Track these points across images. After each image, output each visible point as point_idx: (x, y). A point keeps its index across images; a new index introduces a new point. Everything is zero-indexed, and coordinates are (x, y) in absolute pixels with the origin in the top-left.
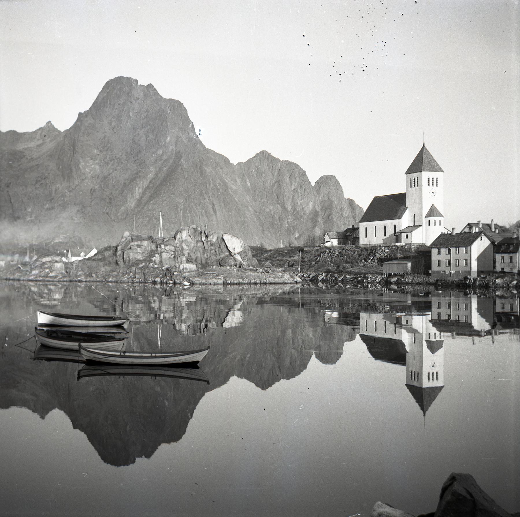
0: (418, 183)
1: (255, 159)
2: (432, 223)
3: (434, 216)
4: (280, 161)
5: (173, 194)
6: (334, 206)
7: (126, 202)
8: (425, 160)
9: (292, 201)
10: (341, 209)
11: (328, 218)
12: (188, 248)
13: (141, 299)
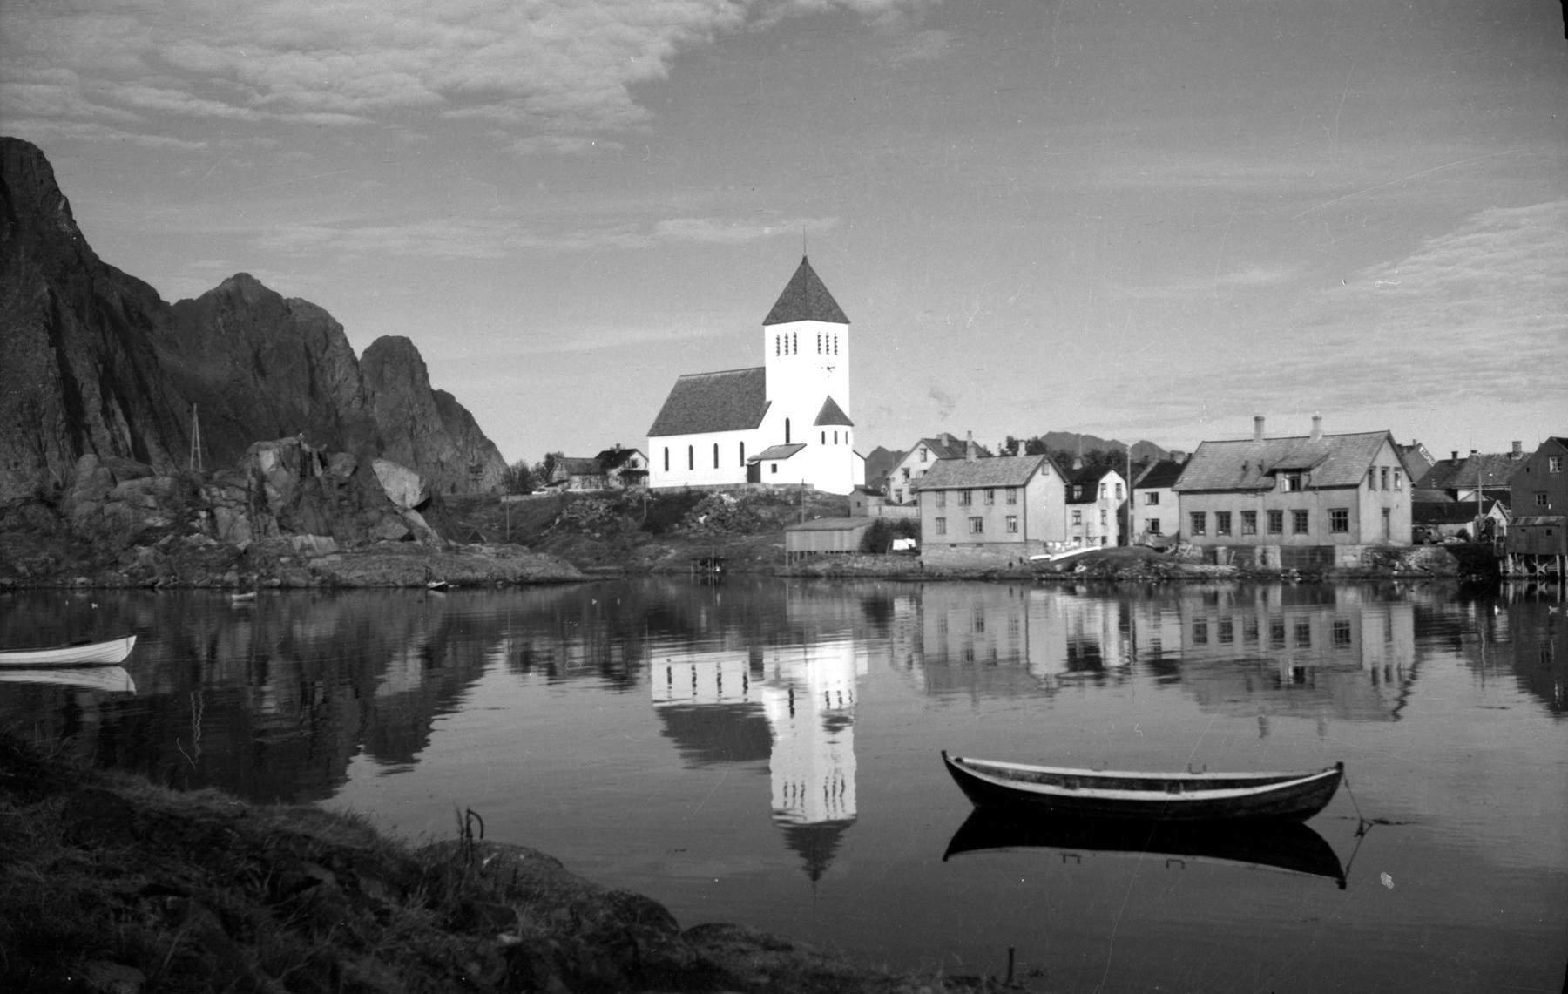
0: (795, 345)
2: (830, 438)
12: (279, 496)
13: (451, 512)
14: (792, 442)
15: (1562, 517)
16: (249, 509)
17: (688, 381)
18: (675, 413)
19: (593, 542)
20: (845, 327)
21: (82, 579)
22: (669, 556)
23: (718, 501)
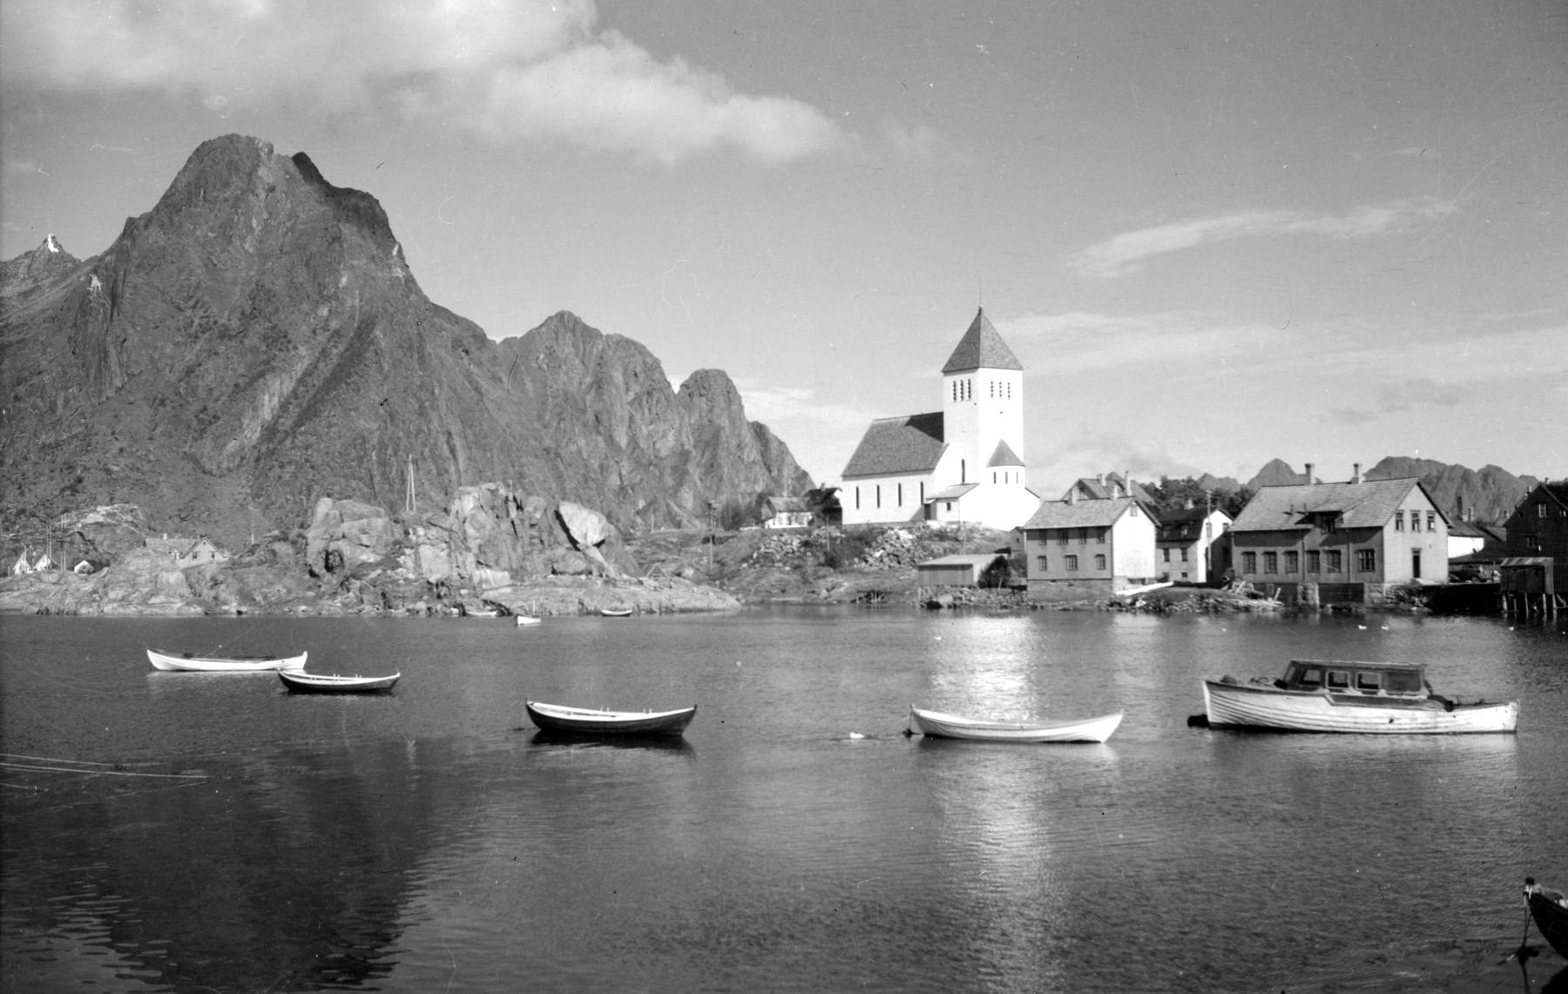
1: (544, 329)
2: (1000, 478)
3: (1004, 464)
4: (601, 336)
5: (356, 410)
6: (724, 439)
7: (241, 427)
8: (985, 342)
9: (630, 427)
10: (739, 446)
11: (712, 465)
13: (671, 546)
14: (966, 482)
15: (1549, 559)
16: (449, 547)
17: (879, 425)
18: (866, 455)
19: (782, 576)
20: (1019, 373)
21: (304, 608)
22: (842, 589)
23: (895, 537)
